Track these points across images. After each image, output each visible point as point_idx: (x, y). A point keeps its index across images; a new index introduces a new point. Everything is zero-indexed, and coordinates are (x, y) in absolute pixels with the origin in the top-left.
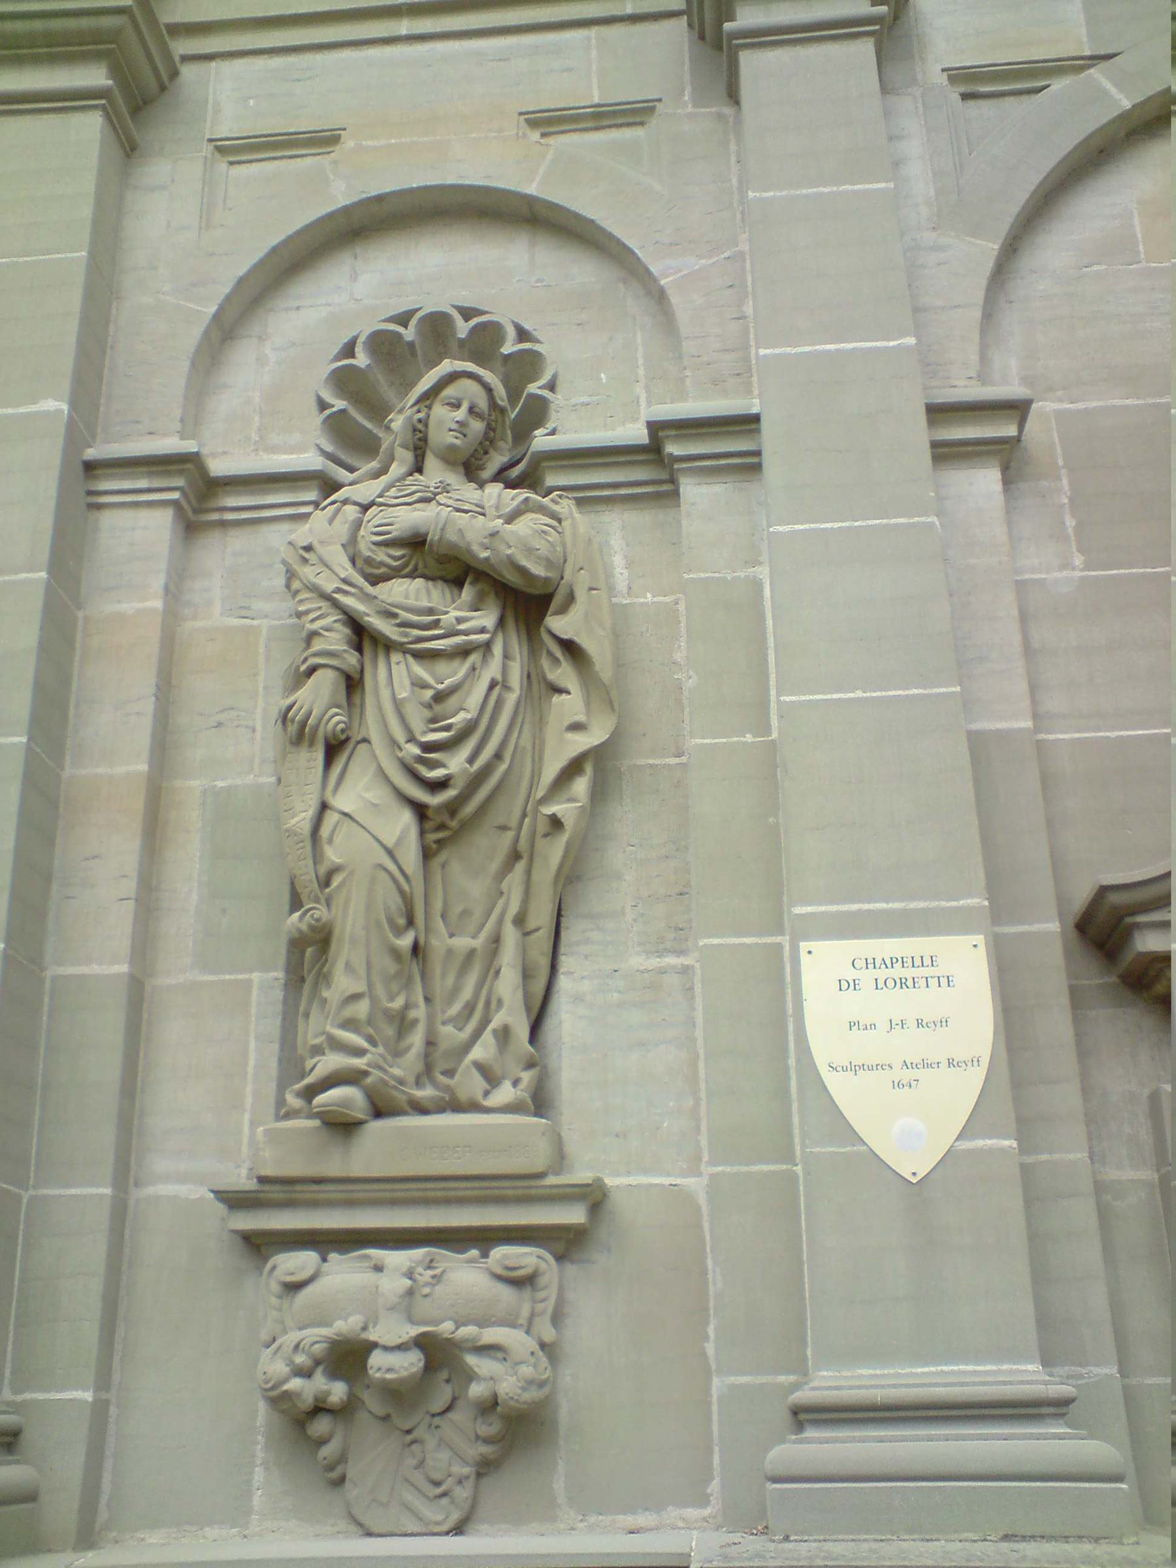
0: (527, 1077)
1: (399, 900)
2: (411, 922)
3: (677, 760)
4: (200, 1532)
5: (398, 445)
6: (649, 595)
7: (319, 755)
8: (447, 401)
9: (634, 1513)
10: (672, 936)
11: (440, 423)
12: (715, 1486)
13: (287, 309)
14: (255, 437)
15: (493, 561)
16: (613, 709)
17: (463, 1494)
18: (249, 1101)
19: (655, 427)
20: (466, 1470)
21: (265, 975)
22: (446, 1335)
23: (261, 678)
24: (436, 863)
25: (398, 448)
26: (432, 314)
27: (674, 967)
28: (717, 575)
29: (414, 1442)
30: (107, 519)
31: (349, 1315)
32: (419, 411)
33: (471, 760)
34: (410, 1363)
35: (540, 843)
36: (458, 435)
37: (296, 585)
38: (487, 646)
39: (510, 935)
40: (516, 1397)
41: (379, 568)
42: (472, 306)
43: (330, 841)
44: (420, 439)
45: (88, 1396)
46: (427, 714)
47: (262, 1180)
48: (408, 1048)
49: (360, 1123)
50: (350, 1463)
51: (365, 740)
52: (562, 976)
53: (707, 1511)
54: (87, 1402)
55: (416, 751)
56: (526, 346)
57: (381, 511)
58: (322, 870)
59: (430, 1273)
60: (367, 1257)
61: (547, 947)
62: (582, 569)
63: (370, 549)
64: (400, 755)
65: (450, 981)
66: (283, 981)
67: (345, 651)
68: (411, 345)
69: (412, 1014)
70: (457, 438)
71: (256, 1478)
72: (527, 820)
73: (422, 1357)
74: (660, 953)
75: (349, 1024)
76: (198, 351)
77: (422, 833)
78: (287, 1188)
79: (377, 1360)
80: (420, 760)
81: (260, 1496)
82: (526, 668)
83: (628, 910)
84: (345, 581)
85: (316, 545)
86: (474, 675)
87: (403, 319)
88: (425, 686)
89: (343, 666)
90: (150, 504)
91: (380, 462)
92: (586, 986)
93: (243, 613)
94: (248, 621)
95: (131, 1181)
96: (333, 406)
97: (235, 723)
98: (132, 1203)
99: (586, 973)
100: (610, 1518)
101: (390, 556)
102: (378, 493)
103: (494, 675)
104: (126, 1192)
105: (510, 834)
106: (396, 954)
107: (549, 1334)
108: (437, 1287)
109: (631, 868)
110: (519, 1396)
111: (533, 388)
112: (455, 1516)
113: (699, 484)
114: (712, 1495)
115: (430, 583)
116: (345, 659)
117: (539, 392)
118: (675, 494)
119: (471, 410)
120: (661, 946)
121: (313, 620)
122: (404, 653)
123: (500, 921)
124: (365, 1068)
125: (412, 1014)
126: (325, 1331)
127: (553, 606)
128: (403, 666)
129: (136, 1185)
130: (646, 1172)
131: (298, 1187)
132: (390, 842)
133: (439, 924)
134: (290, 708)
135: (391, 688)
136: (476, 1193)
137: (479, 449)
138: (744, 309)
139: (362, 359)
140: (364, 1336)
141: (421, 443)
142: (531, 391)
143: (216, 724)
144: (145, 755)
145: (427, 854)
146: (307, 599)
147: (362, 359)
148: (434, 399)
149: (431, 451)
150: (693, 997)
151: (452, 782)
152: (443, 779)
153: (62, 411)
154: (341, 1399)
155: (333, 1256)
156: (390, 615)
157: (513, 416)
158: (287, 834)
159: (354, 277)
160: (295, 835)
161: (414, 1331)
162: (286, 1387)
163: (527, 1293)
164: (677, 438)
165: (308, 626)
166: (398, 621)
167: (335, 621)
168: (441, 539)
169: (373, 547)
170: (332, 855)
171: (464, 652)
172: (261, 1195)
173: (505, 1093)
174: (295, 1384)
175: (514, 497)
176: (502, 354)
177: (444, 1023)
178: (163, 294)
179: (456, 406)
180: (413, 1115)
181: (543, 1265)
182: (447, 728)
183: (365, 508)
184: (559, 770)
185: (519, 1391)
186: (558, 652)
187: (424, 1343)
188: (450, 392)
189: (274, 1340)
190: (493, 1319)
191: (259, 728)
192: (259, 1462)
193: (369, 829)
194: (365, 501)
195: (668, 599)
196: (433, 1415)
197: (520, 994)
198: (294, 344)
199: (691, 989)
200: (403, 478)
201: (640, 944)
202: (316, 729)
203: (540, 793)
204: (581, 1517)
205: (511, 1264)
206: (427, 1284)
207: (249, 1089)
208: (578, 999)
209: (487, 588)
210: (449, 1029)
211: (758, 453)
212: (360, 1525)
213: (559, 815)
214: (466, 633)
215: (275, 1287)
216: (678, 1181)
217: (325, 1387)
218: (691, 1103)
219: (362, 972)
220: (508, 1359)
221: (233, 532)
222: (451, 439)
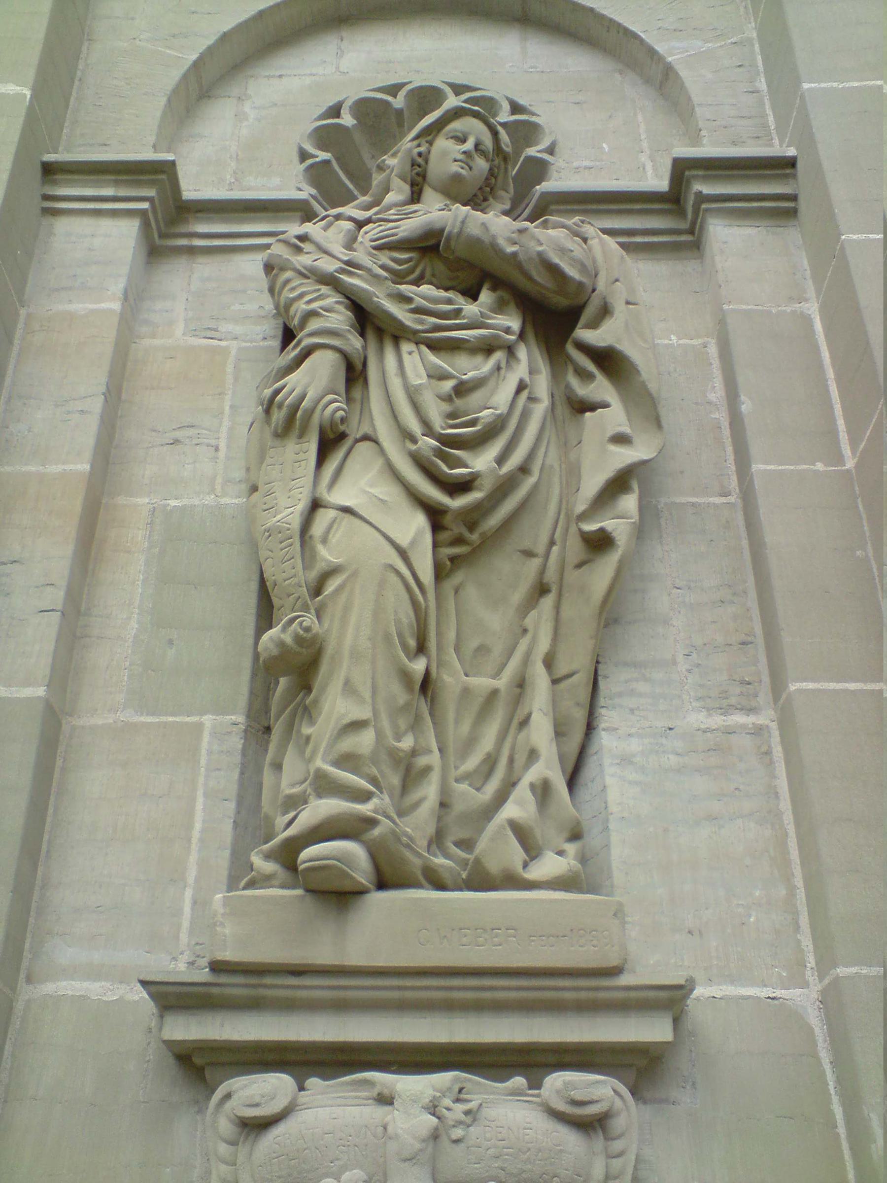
0: (571, 848)
2: (421, 649)
3: (723, 500)
5: (396, 175)
6: (673, 337)
7: (312, 447)
8: (452, 134)
10: (738, 690)
11: (444, 153)
13: (268, 77)
14: (229, 178)
15: (522, 257)
18: (191, 875)
23: (228, 398)
24: (449, 585)
26: (421, 88)
27: (743, 726)
28: (759, 308)
30: (62, 225)
31: (344, 1168)
32: (419, 145)
33: (501, 460)
38: (510, 350)
42: (464, 83)
43: (324, 540)
44: (418, 174)
46: (446, 407)
47: (217, 967)
49: (361, 892)
52: (603, 734)
58: (313, 574)
59: (460, 1107)
61: (584, 695)
62: (617, 280)
65: (465, 728)
67: (349, 331)
68: (399, 113)
69: (422, 761)
70: (462, 168)
72: (555, 549)
74: (726, 711)
75: (347, 761)
76: (176, 91)
77: (435, 545)
78: (253, 980)
82: (550, 391)
83: (680, 658)
86: (499, 374)
87: (393, 90)
88: (443, 376)
90: (114, 213)
91: (372, 196)
92: (634, 746)
93: (209, 334)
94: (215, 342)
95: (22, 976)
96: (317, 157)
97: (196, 441)
98: (19, 1006)
99: (633, 730)
101: (395, 260)
103: (522, 376)
104: (14, 989)
105: (536, 562)
106: (405, 676)
108: (472, 1129)
109: (679, 612)
111: (532, 151)
113: (730, 226)
116: (348, 339)
117: (539, 155)
119: (477, 146)
120: (725, 703)
122: (417, 344)
123: (526, 660)
125: (422, 761)
127: (583, 320)
128: (416, 355)
129: (29, 980)
130: (733, 980)
131: (268, 980)
132: (404, 541)
133: (452, 656)
134: (278, 392)
136: (513, 995)
138: (757, 84)
139: (347, 120)
141: (420, 179)
142: (529, 154)
143: (172, 441)
144: (88, 454)
145: (440, 573)
147: (347, 120)
148: (436, 136)
150: (772, 762)
151: (477, 483)
152: (468, 478)
153: (25, 95)
155: (314, 1082)
157: (514, 172)
159: (340, 54)
163: (599, 1142)
164: (705, 179)
165: (304, 306)
166: (413, 306)
167: (337, 302)
168: (460, 232)
170: (327, 555)
172: (215, 990)
178: (140, 41)
180: (428, 889)
181: (618, 1103)
184: (604, 482)
186: (591, 367)
188: (456, 125)
191: (223, 445)
193: (377, 524)
195: (695, 342)
198: (276, 104)
199: (768, 753)
201: (698, 699)
202: (310, 412)
205: (578, 1095)
207: (193, 858)
208: (625, 760)
209: (506, 296)
210: (464, 787)
211: (794, 198)
213: (609, 529)
215: (225, 1126)
216: (778, 993)
218: (783, 892)
219: (367, 695)
221: (201, 259)
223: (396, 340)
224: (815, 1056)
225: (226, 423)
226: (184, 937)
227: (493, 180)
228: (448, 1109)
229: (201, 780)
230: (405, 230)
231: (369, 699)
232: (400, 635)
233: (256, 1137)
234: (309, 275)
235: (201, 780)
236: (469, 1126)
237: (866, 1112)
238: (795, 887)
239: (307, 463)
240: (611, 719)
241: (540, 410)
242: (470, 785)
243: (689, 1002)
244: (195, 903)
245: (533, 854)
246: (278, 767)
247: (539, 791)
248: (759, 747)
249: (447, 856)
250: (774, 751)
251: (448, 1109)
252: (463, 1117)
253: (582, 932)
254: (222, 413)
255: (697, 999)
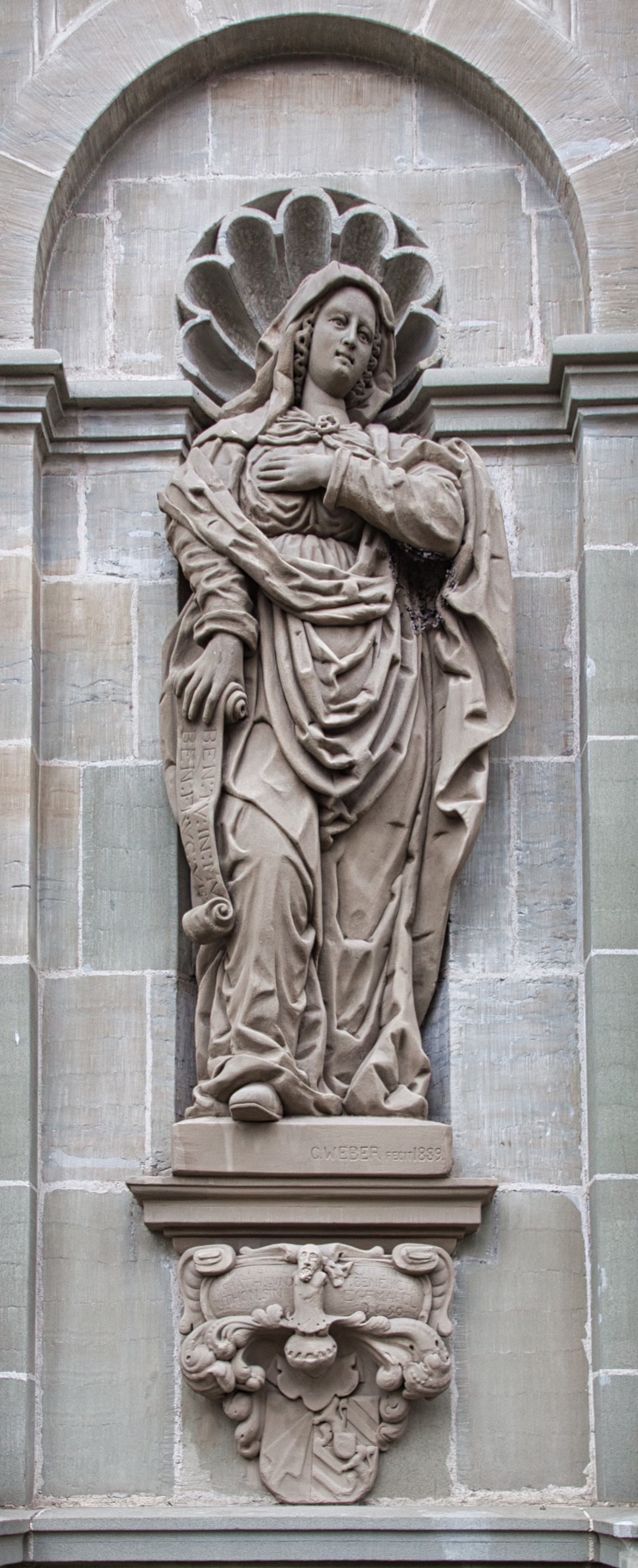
1: (302, 895)
2: (311, 921)
3: (566, 759)
4: (128, 1499)
7: (218, 733)
8: (333, 316)
9: (519, 1490)
12: (591, 1468)
16: (511, 697)
17: (368, 1469)
19: (560, 363)
20: (372, 1448)
21: (157, 972)
22: (358, 1324)
24: (333, 857)
25: (278, 373)
29: (322, 1422)
33: (372, 747)
34: (326, 1348)
35: (433, 844)
36: (347, 360)
37: (182, 536)
38: (385, 618)
39: (403, 938)
40: (423, 1382)
41: (268, 521)
43: (234, 831)
44: (301, 364)
45: (23, 1376)
47: (177, 1174)
48: (313, 1047)
50: (264, 1442)
51: (263, 720)
53: (583, 1490)
54: (22, 1381)
55: (319, 734)
56: (408, 249)
57: (266, 451)
58: (227, 861)
59: (340, 1266)
60: (281, 1251)
61: (437, 953)
63: (257, 497)
64: (303, 738)
65: (346, 984)
66: (175, 979)
67: (245, 616)
68: (279, 239)
69: (313, 1016)
70: (344, 364)
71: (176, 1453)
72: (419, 818)
73: (334, 1343)
75: (257, 1023)
77: (321, 825)
79: (293, 1345)
80: (322, 744)
81: (181, 1469)
84: (241, 533)
85: (208, 491)
88: (327, 661)
89: (243, 634)
100: (498, 1493)
101: (281, 507)
102: (260, 428)
103: (394, 652)
105: (403, 833)
106: (299, 950)
107: (446, 1325)
110: (426, 1380)
111: (416, 306)
112: (361, 1489)
114: (588, 1476)
115: (323, 542)
118: (573, 447)
121: (208, 579)
124: (277, 1066)
126: (248, 1319)
132: (296, 835)
134: (187, 679)
135: (290, 662)
137: (362, 381)
139: (225, 257)
140: (283, 1323)
145: (325, 848)
146: (200, 553)
147: (225, 257)
149: (313, 379)
151: (355, 769)
154: (260, 1381)
155: (246, 1250)
156: (288, 574)
158: (187, 821)
160: (198, 822)
161: (331, 1319)
162: (210, 1370)
163: (428, 1289)
167: (234, 581)
169: (262, 495)
171: (364, 623)
173: (406, 1097)
174: (219, 1368)
175: (409, 444)
176: (382, 259)
177: (339, 1027)
179: (343, 322)
182: (350, 710)
183: (248, 446)
185: (426, 1376)
186: (453, 627)
187: (338, 1331)
189: (192, 1329)
190: (399, 1310)
192: (177, 1439)
194: (247, 438)
196: (341, 1398)
197: (411, 1000)
199: (575, 1000)
200: (284, 413)
202: (215, 704)
203: (439, 787)
204: (471, 1492)
206: (339, 1276)
207: (149, 1087)
210: (344, 1033)
212: (274, 1494)
213: (461, 811)
214: (367, 602)
216: (559, 1188)
217: (246, 1371)
220: (415, 1347)
222: (337, 365)
223: (284, 615)
224: (579, 1231)
225: (136, 677)
226: (148, 1149)
227: (379, 349)
228: (332, 1267)
229: (148, 1025)
230: (290, 474)
231: (273, 974)
232: (295, 917)
233: (211, 1284)
234: (206, 542)
235: (148, 1025)
236: (345, 1278)
237: (599, 1267)
238: (581, 1110)
239: (351, 1423)
240: (252, 1498)
241: (410, 679)
242: (348, 1031)
243: (497, 1194)
244: (153, 1122)
245: (392, 1088)
246: (206, 1016)
247: (398, 1040)
248: (568, 996)
249: (332, 1088)
250: (580, 1002)
251: (332, 1267)
252: (341, 1273)
253: (422, 1150)
254: (132, 665)
255: (503, 1191)
